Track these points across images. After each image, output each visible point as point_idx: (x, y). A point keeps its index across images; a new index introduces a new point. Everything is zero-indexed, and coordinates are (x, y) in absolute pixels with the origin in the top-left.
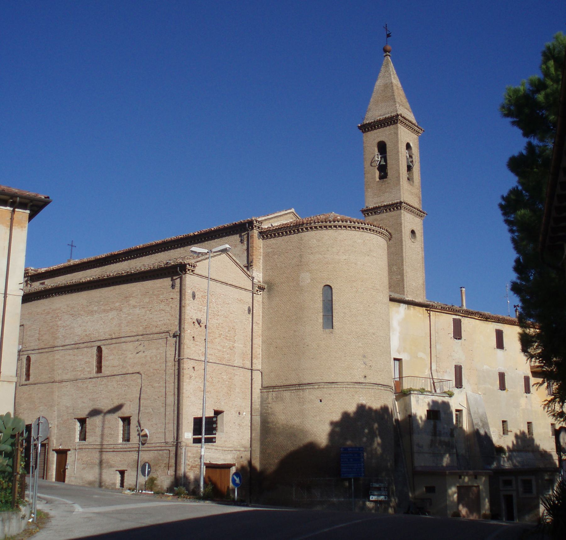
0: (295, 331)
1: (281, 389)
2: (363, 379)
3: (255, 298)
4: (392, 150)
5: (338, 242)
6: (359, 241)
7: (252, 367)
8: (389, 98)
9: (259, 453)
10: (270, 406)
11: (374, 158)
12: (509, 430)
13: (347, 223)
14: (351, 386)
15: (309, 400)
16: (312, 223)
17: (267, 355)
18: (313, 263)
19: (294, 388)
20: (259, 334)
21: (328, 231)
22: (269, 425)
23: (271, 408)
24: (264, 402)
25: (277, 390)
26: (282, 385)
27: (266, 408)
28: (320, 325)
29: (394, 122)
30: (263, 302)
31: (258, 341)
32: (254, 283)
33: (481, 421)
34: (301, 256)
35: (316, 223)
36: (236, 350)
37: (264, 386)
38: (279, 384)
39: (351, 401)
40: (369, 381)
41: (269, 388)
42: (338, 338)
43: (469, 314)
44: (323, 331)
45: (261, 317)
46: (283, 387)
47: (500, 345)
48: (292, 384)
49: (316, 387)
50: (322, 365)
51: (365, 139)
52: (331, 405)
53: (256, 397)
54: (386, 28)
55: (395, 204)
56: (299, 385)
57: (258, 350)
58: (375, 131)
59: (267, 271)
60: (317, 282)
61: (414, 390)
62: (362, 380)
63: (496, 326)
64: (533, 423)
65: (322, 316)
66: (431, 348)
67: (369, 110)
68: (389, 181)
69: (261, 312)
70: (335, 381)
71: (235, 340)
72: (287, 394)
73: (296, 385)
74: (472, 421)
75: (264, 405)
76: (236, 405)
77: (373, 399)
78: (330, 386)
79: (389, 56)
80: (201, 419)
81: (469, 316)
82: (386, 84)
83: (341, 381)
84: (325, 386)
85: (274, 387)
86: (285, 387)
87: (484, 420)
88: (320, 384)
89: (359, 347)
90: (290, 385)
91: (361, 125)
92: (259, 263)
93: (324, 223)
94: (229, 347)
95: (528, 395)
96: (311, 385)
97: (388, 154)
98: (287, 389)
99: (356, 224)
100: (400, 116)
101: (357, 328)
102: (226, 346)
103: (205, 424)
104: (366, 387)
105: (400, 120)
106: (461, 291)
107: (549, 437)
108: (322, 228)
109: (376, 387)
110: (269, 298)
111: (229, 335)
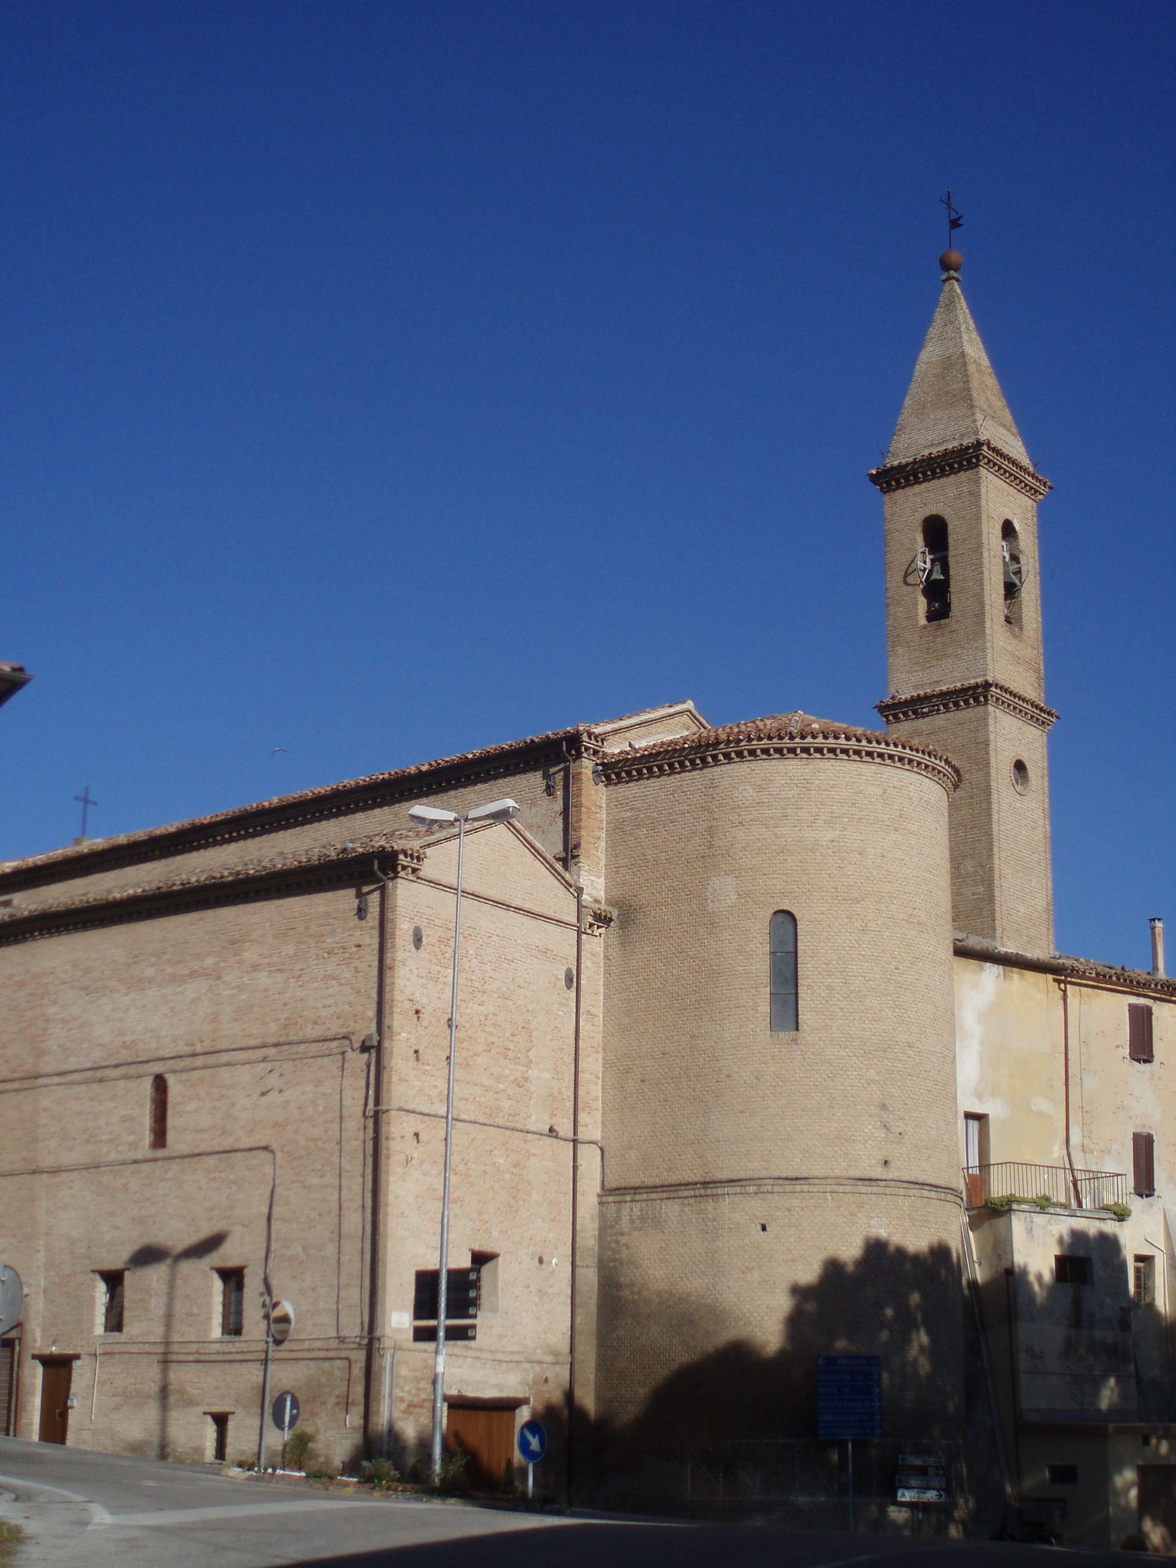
1: (654, 1196)
2: (880, 1169)
3: (586, 946)
4: (965, 540)
7: (575, 1133)
10: (624, 1240)
13: (839, 741)
14: (848, 1189)
15: (732, 1226)
18: (744, 849)
19: (692, 1193)
21: (787, 762)
22: (621, 1294)
23: (628, 1248)
24: (609, 1231)
26: (658, 1182)
30: (606, 958)
31: (592, 1064)
32: (584, 904)
35: (753, 740)
37: (607, 1186)
38: (650, 1182)
40: (896, 1174)
41: (622, 1191)
42: (812, 1057)
45: (602, 998)
46: (660, 1189)
49: (752, 1189)
51: (887, 510)
53: (588, 1217)
55: (969, 688)
56: (705, 1184)
57: (592, 1087)
61: (1020, 1201)
68: (955, 627)
69: (601, 983)
70: (804, 1175)
72: (671, 1210)
73: (696, 1184)
75: (609, 1239)
77: (907, 1224)
78: (789, 1188)
79: (957, 280)
83: (819, 1174)
84: (776, 1189)
85: (636, 1189)
86: (664, 1189)
93: (775, 740)
97: (952, 551)
98: (672, 1195)
99: (864, 743)
100: (985, 448)
101: (864, 1030)
102: (507, 1077)
104: (888, 1191)
110: (623, 944)
111: (512, 1047)
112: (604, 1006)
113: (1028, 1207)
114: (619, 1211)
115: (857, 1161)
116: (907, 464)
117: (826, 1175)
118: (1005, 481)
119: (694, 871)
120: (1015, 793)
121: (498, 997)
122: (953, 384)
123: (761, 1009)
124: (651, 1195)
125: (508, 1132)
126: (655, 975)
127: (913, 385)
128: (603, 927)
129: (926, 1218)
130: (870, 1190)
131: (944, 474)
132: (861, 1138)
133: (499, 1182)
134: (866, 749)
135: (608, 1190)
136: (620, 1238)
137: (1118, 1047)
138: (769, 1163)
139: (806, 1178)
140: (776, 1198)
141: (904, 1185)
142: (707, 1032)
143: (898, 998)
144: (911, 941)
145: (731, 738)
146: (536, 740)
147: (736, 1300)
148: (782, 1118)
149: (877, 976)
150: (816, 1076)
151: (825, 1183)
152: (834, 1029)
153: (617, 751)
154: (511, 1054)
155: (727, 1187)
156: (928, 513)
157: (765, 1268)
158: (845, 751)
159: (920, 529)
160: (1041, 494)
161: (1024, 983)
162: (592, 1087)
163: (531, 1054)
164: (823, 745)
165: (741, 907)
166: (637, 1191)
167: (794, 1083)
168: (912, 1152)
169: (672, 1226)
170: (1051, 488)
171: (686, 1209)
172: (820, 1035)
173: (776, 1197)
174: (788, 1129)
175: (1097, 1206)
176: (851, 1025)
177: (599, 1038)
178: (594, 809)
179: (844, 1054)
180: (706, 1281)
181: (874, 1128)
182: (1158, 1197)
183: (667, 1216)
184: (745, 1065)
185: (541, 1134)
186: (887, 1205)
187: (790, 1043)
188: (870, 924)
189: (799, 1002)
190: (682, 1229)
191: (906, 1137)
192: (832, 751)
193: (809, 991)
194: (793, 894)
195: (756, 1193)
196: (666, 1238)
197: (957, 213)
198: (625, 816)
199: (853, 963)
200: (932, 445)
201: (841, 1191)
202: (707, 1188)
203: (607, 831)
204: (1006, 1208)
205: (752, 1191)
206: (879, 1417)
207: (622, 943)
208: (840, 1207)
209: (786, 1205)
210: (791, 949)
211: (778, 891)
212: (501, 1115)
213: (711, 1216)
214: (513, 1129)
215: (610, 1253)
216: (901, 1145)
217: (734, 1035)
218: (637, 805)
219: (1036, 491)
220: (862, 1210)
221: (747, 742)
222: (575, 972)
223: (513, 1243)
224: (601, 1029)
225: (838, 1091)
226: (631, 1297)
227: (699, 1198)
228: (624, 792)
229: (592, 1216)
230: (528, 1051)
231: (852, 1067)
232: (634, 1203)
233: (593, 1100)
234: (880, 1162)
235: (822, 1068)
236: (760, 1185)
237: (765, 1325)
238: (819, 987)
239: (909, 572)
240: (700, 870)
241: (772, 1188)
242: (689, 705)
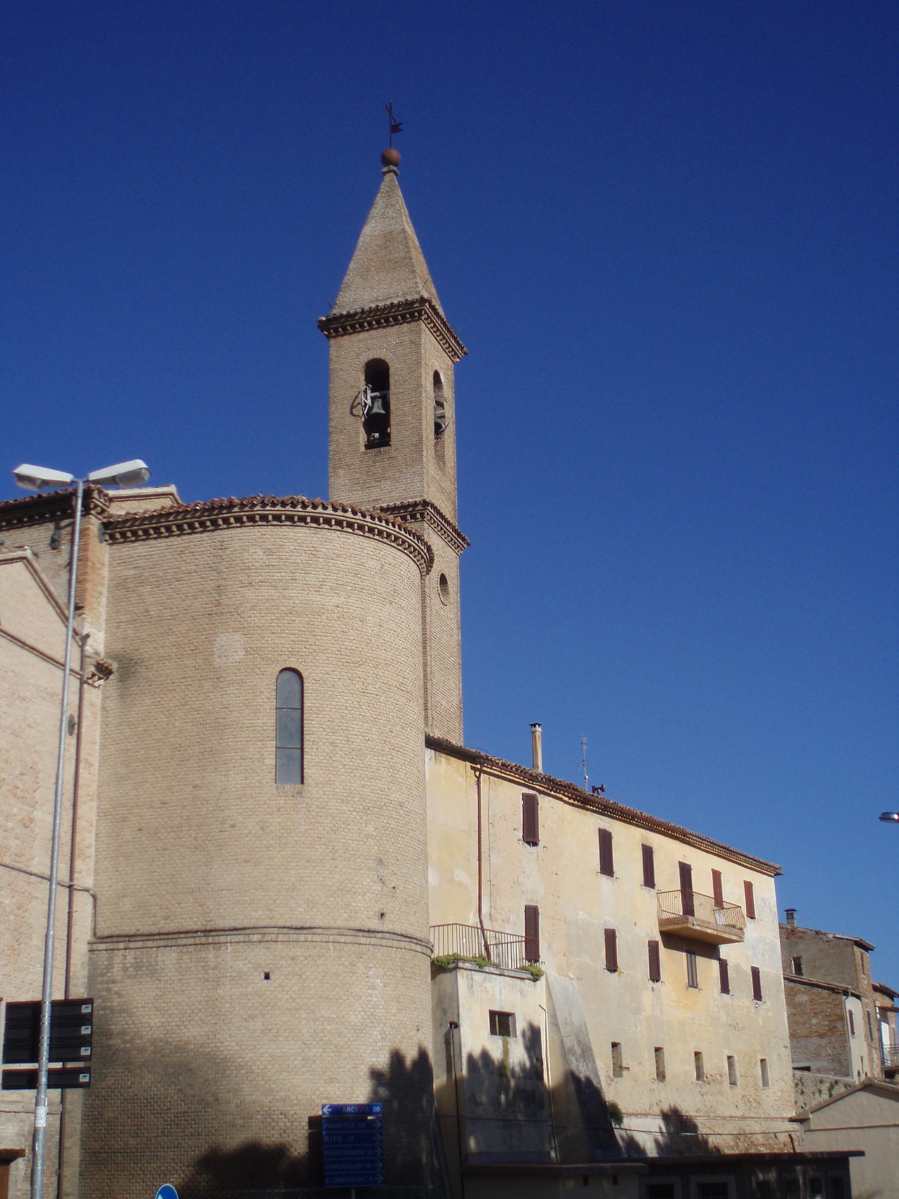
0: (195, 787)
1: (150, 944)
2: (377, 921)
3: (86, 696)
4: (405, 381)
5: (321, 560)
6: (372, 564)
7: (71, 879)
8: (397, 262)
9: (79, 1120)
10: (115, 988)
11: (357, 397)
12: (624, 1065)
13: (346, 515)
14: (349, 939)
15: (234, 974)
16: (255, 505)
17: (112, 848)
18: (253, 608)
19: (192, 941)
20: (91, 793)
21: (297, 529)
22: (111, 1042)
23: (120, 996)
24: (100, 979)
25: (140, 944)
26: (155, 930)
27: (104, 993)
28: (270, 772)
29: (412, 315)
30: (104, 709)
31: (88, 811)
32: (87, 654)
33: (579, 1041)
34: (219, 590)
35: (267, 505)
36: (37, 830)
37: (99, 934)
38: (146, 930)
39: (348, 978)
40: (390, 926)
41: (115, 939)
42: (317, 810)
43: (554, 787)
44: (277, 788)
45: (98, 748)
46: (156, 937)
47: (607, 867)
48: (184, 929)
49: (256, 938)
50: (273, 880)
51: (333, 353)
52: (295, 988)
53: (79, 964)
54: (390, 109)
55: (409, 506)
56: (207, 932)
57: (87, 835)
58: (363, 335)
59: (118, 627)
60: (263, 659)
61: (464, 960)
62: (375, 924)
63: (599, 821)
64: (665, 1050)
65: (274, 749)
66: (480, 860)
67: (345, 287)
68: (394, 454)
69: (98, 733)
70: (308, 925)
71: (37, 803)
72: (168, 958)
73: (196, 932)
74: (562, 1041)
75: (99, 986)
76: (31, 984)
77: (399, 975)
78: (293, 937)
79: (396, 174)
80: (35, 1007)
81: (552, 793)
82: (391, 233)
83: (322, 925)
84: (281, 938)
85: (130, 937)
86: (162, 937)
87: (584, 1040)
88: (265, 930)
89: (368, 836)
90: (179, 933)
91: (328, 320)
92: (99, 603)
93: (288, 508)
94: (20, 818)
95: (656, 985)
96: (242, 932)
97: (393, 390)
98: (170, 943)
99: (368, 519)
100: (427, 305)
101: (363, 786)
102: (15, 815)
103: (52, 1025)
104: (384, 942)
105: (426, 313)
106: (534, 732)
107: (692, 1082)
108: (281, 521)
109: (407, 945)
110: (122, 697)
111: (20, 786)
112: (100, 756)
113: (470, 965)
114: (111, 958)
115: (357, 913)
116: (356, 314)
117: (328, 925)
118: (436, 339)
119: (200, 627)
120: (440, 601)
121: (11, 734)
122: (395, 253)
123: (267, 761)
124: (147, 942)
125: (14, 873)
126: (155, 726)
127: (357, 253)
128: (102, 679)
129: (413, 970)
130: (368, 941)
131: (388, 324)
132: (361, 891)
133: (5, 923)
134: (369, 524)
135: (99, 938)
136: (110, 986)
137: (515, 829)
138: (274, 913)
139: (310, 928)
140: (280, 947)
141: (399, 938)
142: (210, 783)
143: (392, 759)
144: (402, 707)
145: (244, 502)
146: (44, 495)
147: (237, 1048)
148: (286, 869)
149: (375, 737)
150: (320, 828)
151: (329, 933)
152: (337, 783)
153: (123, 513)
154: (20, 794)
155: (231, 935)
156: (371, 357)
157: (268, 1016)
158: (350, 525)
159: (363, 370)
160: (458, 357)
161: (449, 767)
162: (87, 835)
163: (37, 795)
164: (331, 517)
165: (249, 663)
166: (132, 939)
167: (299, 834)
168: (403, 907)
169: (169, 974)
170: (465, 354)
171: (185, 957)
172: (324, 789)
173: (280, 946)
174: (292, 879)
175: (518, 966)
176: (352, 781)
177: (94, 786)
178: (98, 565)
179: (345, 808)
180: (206, 1029)
181: (372, 881)
182: (542, 962)
183: (164, 964)
184: (250, 815)
185: (42, 878)
186: (382, 956)
187: (295, 795)
188: (370, 687)
189: (305, 756)
190: (180, 977)
191: (398, 891)
192: (339, 523)
193: (314, 747)
194: (301, 654)
195: (260, 942)
196: (162, 986)
197: (395, 121)
198: (128, 574)
199: (355, 723)
200: (377, 300)
201: (343, 941)
202: (208, 936)
203: (108, 588)
204: (451, 966)
205: (255, 940)
206: (380, 1165)
207: (120, 695)
208: (341, 957)
209: (291, 954)
210: (298, 706)
211: (285, 650)
212: (8, 854)
213: (212, 964)
214: (19, 870)
215: (100, 1001)
216: (394, 899)
217: (239, 786)
218: (142, 563)
219: (456, 354)
220: (361, 960)
221: (261, 507)
222: (76, 720)
223: (15, 987)
224: (96, 778)
225: (340, 844)
226: (122, 1046)
227: (199, 946)
228: (128, 551)
229: (83, 963)
230: (34, 792)
231: (353, 821)
232: (128, 951)
233: (87, 847)
234: (377, 914)
235: (326, 821)
236: (265, 934)
237: (269, 1074)
238: (324, 743)
239: (355, 405)
240: (206, 626)
241: (277, 937)
242: (172, 489)
